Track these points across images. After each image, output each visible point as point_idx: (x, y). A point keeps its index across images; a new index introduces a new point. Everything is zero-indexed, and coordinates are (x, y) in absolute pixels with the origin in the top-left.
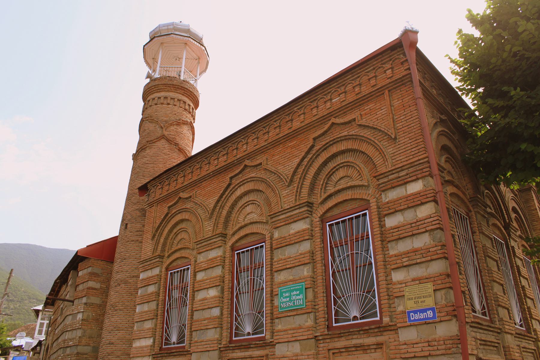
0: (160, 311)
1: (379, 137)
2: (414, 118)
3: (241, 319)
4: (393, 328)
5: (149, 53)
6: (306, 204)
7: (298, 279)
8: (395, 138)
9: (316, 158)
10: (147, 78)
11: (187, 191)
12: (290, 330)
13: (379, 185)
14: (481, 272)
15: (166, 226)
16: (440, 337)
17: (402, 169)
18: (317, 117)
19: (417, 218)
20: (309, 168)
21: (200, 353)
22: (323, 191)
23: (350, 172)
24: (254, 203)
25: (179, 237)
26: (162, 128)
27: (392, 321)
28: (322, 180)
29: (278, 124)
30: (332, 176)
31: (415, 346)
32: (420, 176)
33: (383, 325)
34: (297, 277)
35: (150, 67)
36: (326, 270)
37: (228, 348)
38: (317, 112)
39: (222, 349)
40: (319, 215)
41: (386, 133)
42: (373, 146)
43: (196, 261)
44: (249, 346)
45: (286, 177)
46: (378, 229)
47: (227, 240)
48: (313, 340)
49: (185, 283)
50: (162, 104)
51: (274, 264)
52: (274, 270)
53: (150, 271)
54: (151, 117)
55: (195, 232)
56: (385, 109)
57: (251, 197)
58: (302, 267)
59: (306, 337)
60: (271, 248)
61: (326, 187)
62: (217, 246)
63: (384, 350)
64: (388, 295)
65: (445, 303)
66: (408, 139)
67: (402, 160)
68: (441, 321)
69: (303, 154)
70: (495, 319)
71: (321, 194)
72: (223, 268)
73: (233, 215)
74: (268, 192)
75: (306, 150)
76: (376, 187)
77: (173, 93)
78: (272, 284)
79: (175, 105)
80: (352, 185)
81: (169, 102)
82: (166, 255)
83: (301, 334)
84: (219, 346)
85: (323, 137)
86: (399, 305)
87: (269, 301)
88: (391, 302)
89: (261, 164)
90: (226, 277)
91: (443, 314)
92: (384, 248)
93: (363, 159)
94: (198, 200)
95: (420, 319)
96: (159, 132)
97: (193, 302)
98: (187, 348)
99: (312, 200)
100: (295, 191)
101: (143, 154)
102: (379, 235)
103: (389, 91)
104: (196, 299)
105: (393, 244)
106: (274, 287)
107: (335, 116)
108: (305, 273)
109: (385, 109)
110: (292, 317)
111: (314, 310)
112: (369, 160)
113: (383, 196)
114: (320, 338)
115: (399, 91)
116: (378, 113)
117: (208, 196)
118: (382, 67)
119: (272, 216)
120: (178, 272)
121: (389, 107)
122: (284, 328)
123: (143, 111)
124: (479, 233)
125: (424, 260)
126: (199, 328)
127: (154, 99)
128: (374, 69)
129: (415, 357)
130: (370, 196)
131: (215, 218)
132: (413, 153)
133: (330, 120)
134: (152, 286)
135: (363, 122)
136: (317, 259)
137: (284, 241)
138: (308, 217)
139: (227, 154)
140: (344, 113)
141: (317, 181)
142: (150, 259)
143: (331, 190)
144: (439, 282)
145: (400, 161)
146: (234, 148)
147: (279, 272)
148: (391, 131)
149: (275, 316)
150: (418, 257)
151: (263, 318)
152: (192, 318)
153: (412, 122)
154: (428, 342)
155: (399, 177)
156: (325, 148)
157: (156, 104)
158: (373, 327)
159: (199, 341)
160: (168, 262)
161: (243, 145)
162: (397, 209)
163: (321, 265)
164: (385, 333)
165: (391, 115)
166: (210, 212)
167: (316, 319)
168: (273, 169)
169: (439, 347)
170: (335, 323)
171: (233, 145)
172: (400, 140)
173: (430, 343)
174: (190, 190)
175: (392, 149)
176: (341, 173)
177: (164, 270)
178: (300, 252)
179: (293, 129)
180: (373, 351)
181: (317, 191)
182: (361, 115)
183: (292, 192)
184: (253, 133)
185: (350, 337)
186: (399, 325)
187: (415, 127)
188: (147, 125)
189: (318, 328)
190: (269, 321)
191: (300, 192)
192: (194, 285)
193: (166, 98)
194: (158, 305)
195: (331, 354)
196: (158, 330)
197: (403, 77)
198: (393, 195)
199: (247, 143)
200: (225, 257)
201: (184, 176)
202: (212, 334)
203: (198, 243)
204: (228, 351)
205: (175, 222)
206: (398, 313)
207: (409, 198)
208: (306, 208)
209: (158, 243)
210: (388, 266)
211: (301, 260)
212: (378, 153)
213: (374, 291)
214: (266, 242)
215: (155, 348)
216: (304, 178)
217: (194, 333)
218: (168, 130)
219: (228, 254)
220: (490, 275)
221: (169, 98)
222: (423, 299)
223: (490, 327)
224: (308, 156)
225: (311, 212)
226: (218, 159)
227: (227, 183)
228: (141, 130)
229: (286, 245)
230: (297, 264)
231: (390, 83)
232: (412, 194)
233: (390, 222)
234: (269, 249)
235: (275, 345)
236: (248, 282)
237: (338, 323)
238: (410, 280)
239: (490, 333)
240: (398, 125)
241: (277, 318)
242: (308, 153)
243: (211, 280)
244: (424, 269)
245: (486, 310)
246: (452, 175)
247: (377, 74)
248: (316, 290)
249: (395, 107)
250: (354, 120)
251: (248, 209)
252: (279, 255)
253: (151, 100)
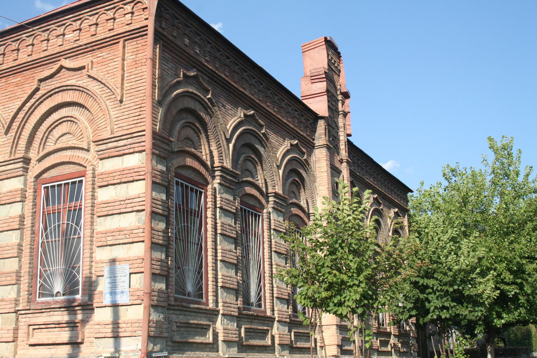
17: (120, 138)
38: (47, 46)
67: (124, 128)
85: (50, 80)
93: (88, 116)
115: (135, 43)
116: (110, 65)
130: (87, 162)
133: (59, 60)
143: (50, 146)
150: (122, 237)
151: (79, 275)
156: (50, 94)
208: (20, 165)
214: (87, 176)
224: (31, 101)
236: (55, 230)
247: (116, 15)
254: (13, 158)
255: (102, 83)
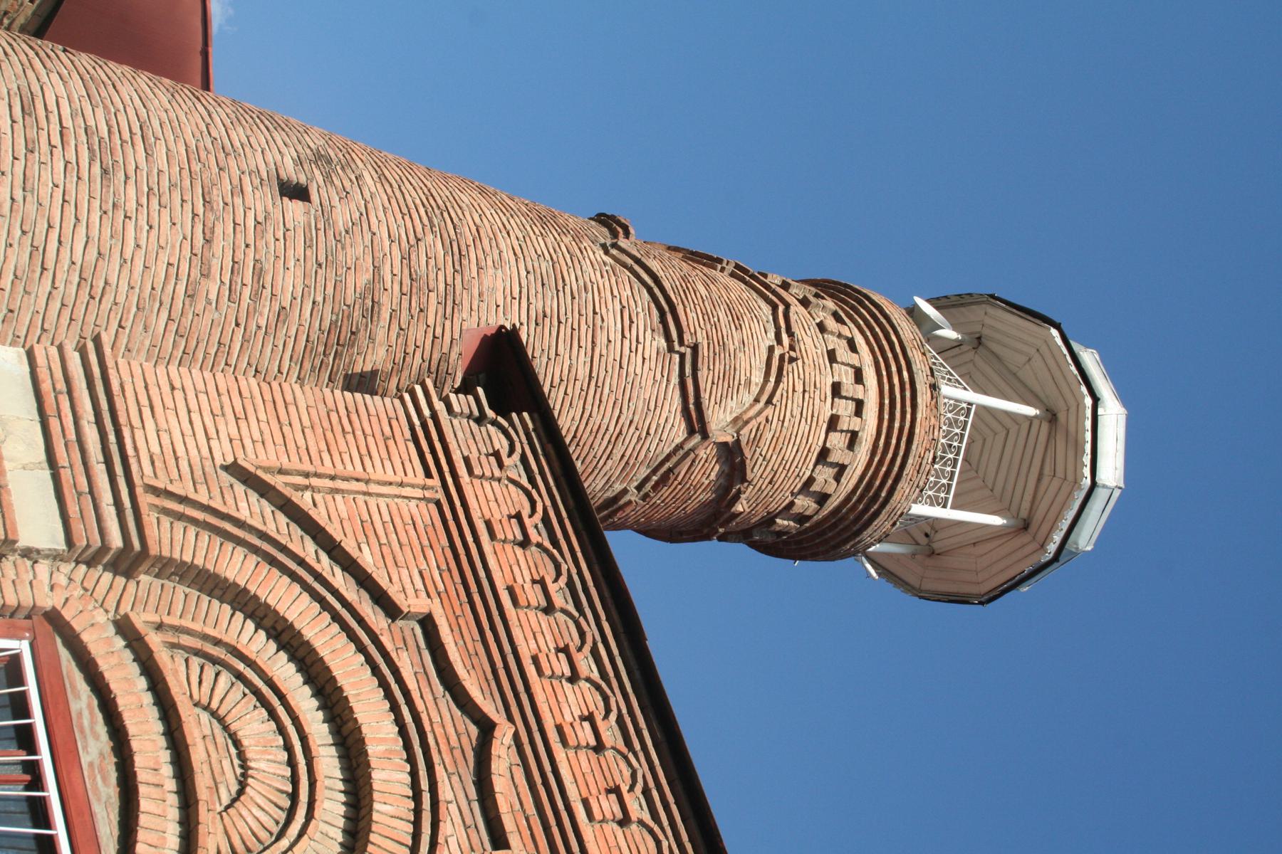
38: (578, 747)
254: (144, 509)
255: (234, 800)
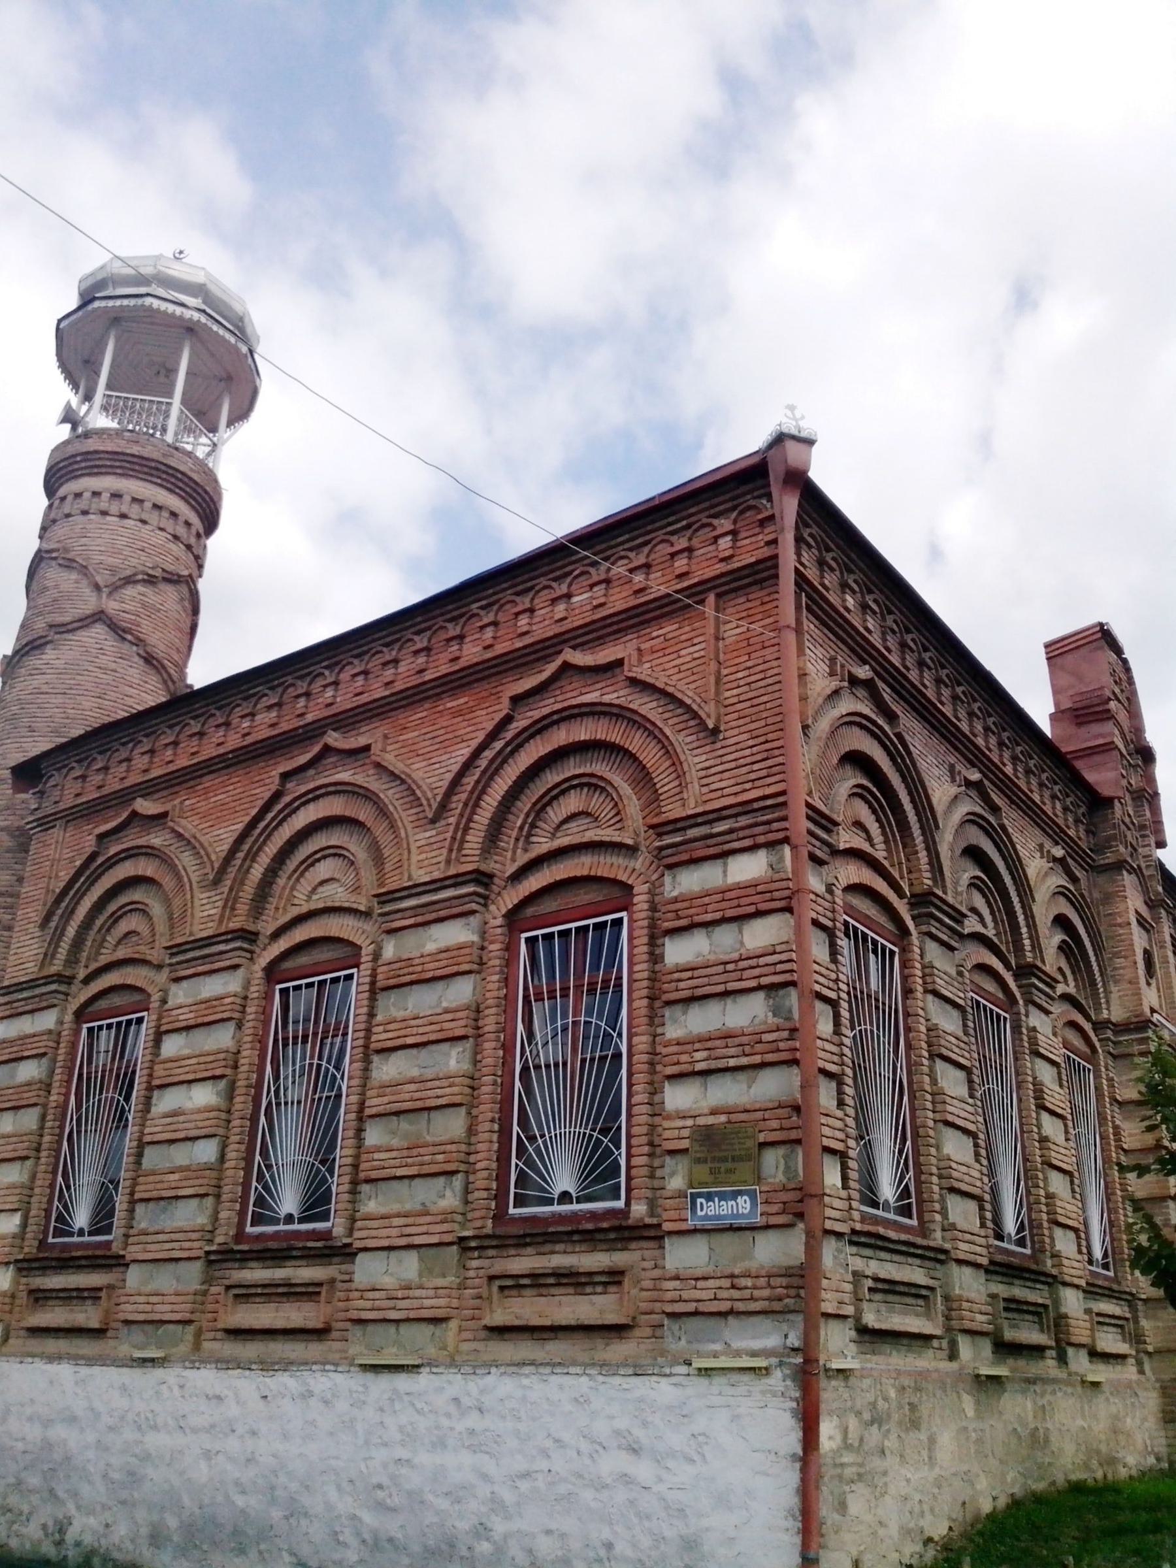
0: (47, 1139)
1: (676, 720)
2: (770, 681)
3: (272, 1177)
4: (651, 1234)
5: (76, 350)
6: (473, 876)
7: (430, 1077)
8: (715, 731)
9: (512, 753)
10: (65, 420)
11: (156, 796)
12: (398, 1215)
13: (661, 849)
14: (912, 1098)
15: (88, 889)
16: (763, 1267)
17: (718, 815)
18: (528, 640)
19: (743, 951)
20: (491, 778)
21: (150, 1266)
22: (521, 844)
23: (596, 802)
24: (340, 855)
25: (123, 926)
26: (97, 588)
27: (652, 1215)
28: (522, 816)
29: (425, 644)
30: (549, 809)
31: (700, 1284)
32: (761, 839)
33: (630, 1222)
34: (429, 1073)
35: (75, 386)
36: (507, 1062)
37: (229, 1256)
39: (213, 1257)
40: (504, 911)
41: (696, 713)
42: (660, 741)
43: (164, 1001)
44: (286, 1253)
45: (430, 795)
46: (644, 966)
47: (258, 950)
48: (455, 1247)
49: (129, 1061)
50: (104, 513)
51: (375, 1030)
52: (373, 1046)
53: (28, 1017)
54: (66, 550)
55: (171, 918)
56: (703, 646)
57: (334, 838)
58: (445, 1047)
59: (434, 1239)
60: (373, 983)
61: (529, 835)
62: (228, 963)
63: (626, 1290)
64: (651, 1144)
65: (784, 1180)
66: (745, 736)
67: (726, 792)
68: (767, 1227)
69: (481, 736)
70: (932, 1226)
71: (514, 852)
72: (239, 1026)
73: (281, 882)
74: (380, 830)
75: (490, 726)
76: (655, 853)
77: (141, 483)
78: (365, 1086)
79: (144, 522)
80: (597, 838)
81: (124, 509)
82: (82, 974)
83: (424, 1229)
84: (207, 1248)
86: (673, 1174)
87: (351, 1133)
88: (656, 1163)
89: (367, 748)
90: (244, 1053)
91: (774, 1208)
92: (654, 1019)
94: (187, 826)
95: (719, 1217)
96: (89, 602)
97: (144, 1119)
98: (116, 1248)
99: (490, 866)
100: (449, 835)
101: (33, 661)
102: (645, 983)
103: (718, 596)
104: (153, 1109)
105: (678, 1009)
106: (369, 1093)
107: (573, 643)
108: (453, 1063)
109: (703, 646)
110: (406, 1181)
111: (463, 1167)
112: (643, 778)
113: (667, 879)
114: (473, 1244)
116: (683, 652)
117: (212, 821)
118: (710, 525)
119: (385, 898)
120: (109, 1026)
121: (713, 641)
122: (383, 1210)
123: (44, 529)
124: (926, 991)
125: (744, 1061)
126: (155, 1194)
127: (78, 495)
128: (688, 526)
129: (696, 1313)
131: (229, 883)
132: (753, 776)
134: (30, 1061)
135: (643, 672)
136: (486, 1029)
137: (406, 971)
138: (473, 912)
139: (279, 705)
140: (599, 638)
141: (510, 817)
142: (32, 984)
143: (543, 844)
144: (775, 1124)
145: (719, 793)
146: (300, 691)
147: (386, 1054)
148: (706, 709)
149: (362, 1175)
150: (732, 1051)
152: (138, 1163)
153: (762, 691)
154: (732, 1276)
155: (712, 836)
157: (85, 513)
158: (605, 1225)
159: (151, 1230)
160: (83, 997)
161: (325, 686)
162: (697, 919)
163: (493, 1044)
164: (633, 1245)
165: (713, 666)
166: (216, 865)
167: (467, 1191)
168: (398, 767)
169: (756, 1293)
170: (515, 1207)
171: (299, 683)
172: (728, 734)
173: (736, 1281)
174: (165, 793)
175: (704, 757)
176: (573, 802)
177: (69, 1018)
178: (445, 1004)
179: (462, 663)
180: (599, 1289)
181: (507, 841)
182: (639, 650)
183: (441, 837)
184: (356, 657)
185: (548, 1247)
186: (667, 1226)
187: (768, 706)
188: (52, 574)
189: (470, 1216)
190: (346, 1187)
191: (463, 841)
192: (151, 1068)
193: (116, 496)
194: (43, 1118)
195: (495, 1289)
196: (37, 1191)
197: (758, 562)
198: (691, 881)
199: (336, 683)
200: (245, 998)
201: (152, 752)
202: (190, 1215)
203: (174, 950)
204: (229, 1265)
205: (114, 881)
206: (669, 1194)
207: (728, 895)
209: (60, 939)
210: (659, 1068)
211: (446, 1025)
212: (668, 763)
213: (619, 1128)
214: (362, 967)
215: (26, 1243)
216: (477, 805)
217: (140, 1209)
218: (117, 596)
219: (255, 991)
220: (939, 1107)
221: (127, 498)
222: (730, 1165)
223: (914, 1245)
225: (486, 898)
226: (253, 715)
227: (274, 788)
228: (34, 586)
229: (412, 983)
230: (433, 1037)
231: (722, 575)
232: (738, 887)
233: (680, 952)
234: (367, 987)
235: (356, 1254)
237: (521, 1206)
238: (706, 1111)
239: (910, 1260)
240: (728, 694)
241: (368, 1181)
242: (493, 736)
243: (202, 1059)
244: (745, 1086)
245: (913, 1200)
246: (866, 831)
248: (475, 1112)
249: (728, 642)
250: (619, 663)
251: (324, 869)
252: (392, 1007)
253: (70, 498)
